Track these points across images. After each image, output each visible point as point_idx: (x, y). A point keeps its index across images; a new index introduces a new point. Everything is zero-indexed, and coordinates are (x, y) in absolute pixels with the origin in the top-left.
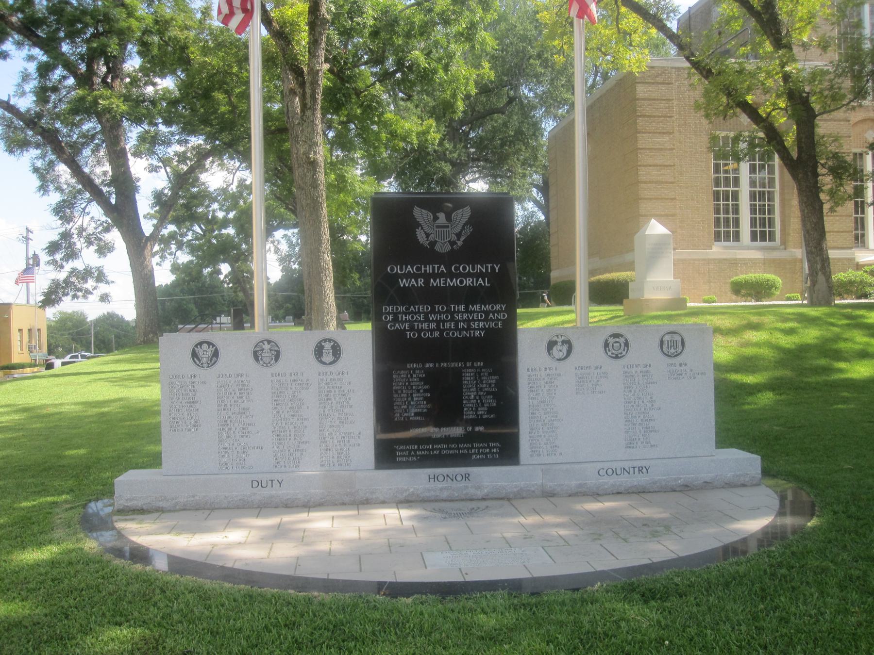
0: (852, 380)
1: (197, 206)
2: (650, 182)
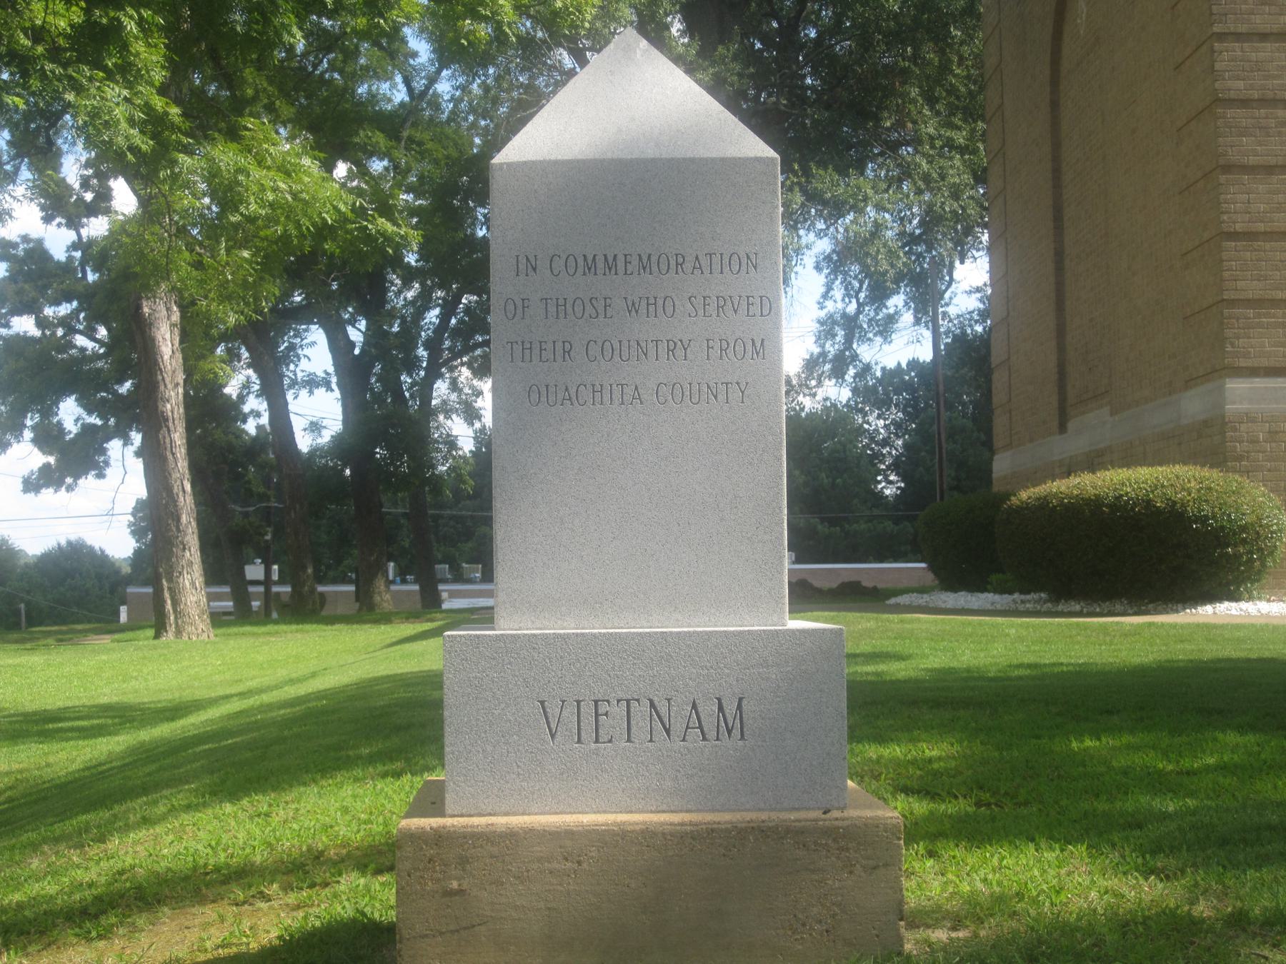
0: (335, 365)
1: (15, 399)
2: (1264, 102)
